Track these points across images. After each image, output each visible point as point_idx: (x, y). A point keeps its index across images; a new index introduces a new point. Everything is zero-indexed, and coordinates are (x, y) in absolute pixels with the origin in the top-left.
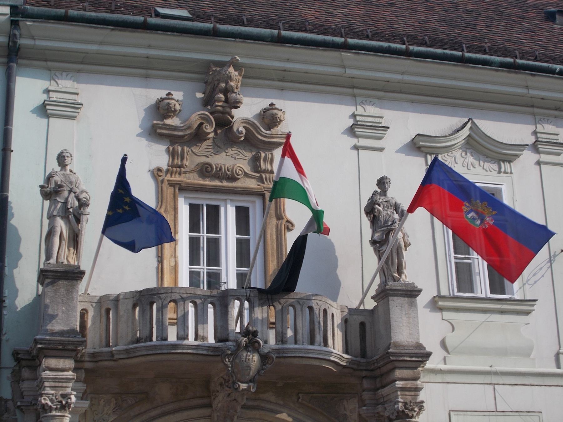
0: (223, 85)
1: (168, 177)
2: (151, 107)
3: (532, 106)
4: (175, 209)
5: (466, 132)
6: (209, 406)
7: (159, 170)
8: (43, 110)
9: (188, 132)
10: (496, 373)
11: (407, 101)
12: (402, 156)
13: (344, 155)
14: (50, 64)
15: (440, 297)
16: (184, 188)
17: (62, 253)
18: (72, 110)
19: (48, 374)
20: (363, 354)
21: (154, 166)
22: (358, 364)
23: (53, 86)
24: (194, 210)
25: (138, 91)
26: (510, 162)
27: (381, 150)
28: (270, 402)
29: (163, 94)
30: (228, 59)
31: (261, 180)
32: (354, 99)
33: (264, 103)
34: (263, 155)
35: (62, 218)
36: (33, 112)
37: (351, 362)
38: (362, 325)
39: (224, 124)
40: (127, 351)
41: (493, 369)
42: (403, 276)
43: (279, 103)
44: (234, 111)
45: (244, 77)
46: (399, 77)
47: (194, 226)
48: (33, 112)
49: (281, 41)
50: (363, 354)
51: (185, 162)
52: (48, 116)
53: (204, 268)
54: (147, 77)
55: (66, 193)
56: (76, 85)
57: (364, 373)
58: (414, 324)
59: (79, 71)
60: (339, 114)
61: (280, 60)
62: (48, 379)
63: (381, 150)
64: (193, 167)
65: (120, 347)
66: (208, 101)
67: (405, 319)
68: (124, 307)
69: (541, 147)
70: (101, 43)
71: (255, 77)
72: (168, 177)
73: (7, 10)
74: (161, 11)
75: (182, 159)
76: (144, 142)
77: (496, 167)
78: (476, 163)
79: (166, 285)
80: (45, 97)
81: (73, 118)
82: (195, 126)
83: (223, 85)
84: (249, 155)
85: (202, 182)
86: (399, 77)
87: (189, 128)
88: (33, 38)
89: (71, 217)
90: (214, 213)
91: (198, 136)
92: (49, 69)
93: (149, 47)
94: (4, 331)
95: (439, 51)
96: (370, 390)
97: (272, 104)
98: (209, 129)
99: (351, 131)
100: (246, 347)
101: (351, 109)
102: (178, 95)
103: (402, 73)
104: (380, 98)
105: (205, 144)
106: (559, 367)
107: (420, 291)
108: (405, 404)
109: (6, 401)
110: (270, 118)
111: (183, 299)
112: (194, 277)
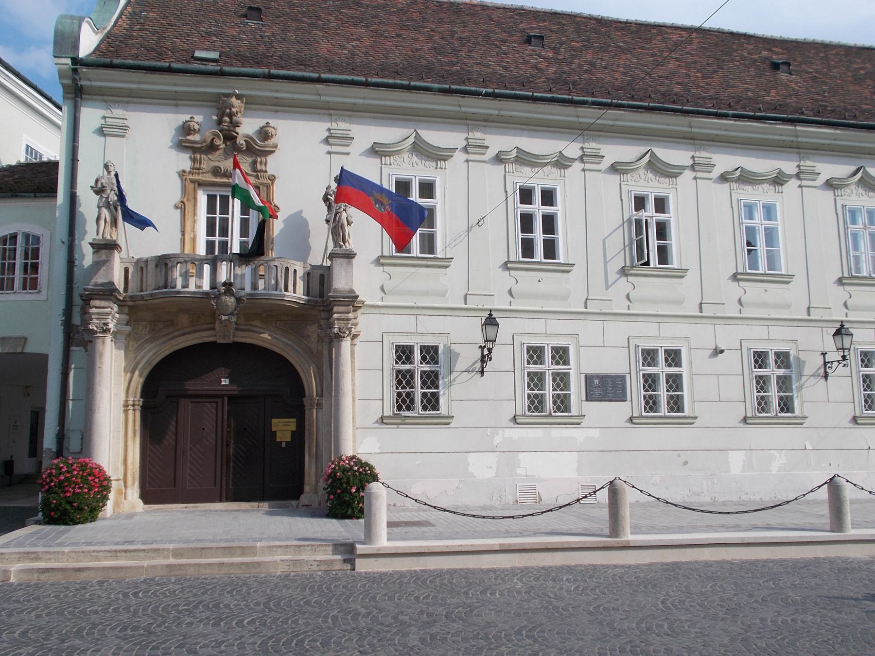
0: (228, 111)
1: (190, 177)
2: (179, 127)
3: (466, 119)
4: (195, 199)
5: (859, 175)
6: (214, 329)
7: (184, 171)
8: (101, 132)
9: (204, 144)
10: (418, 308)
11: (370, 117)
12: (364, 158)
13: (301, 159)
14: (106, 98)
15: (382, 257)
16: (201, 184)
17: (106, 232)
18: (122, 131)
19: (94, 310)
20: (321, 295)
21: (180, 169)
22: (317, 302)
23: (108, 113)
24: (211, 199)
25: (171, 116)
26: (445, 161)
27: (348, 154)
28: (256, 326)
29: (187, 117)
30: (230, 91)
31: (257, 177)
32: (330, 117)
33: (261, 122)
34: (259, 159)
35: (106, 208)
36: (94, 132)
37: (308, 301)
38: (322, 276)
39: (230, 137)
40: (151, 295)
41: (416, 305)
42: (347, 244)
43: (273, 122)
44: (237, 130)
45: (246, 103)
46: (361, 101)
47: (211, 209)
48: (94, 132)
49: (270, 77)
50: (321, 295)
51: (202, 165)
52: (105, 135)
53: (217, 239)
54: (177, 105)
55: (109, 191)
56: (125, 113)
57: (322, 308)
58: (350, 275)
59: (127, 102)
60: (318, 128)
61: (271, 91)
62: (94, 314)
63: (348, 154)
64: (209, 169)
65: (148, 292)
66: (220, 122)
67: (343, 273)
68: (151, 266)
69: (802, 176)
70: (139, 83)
71: (252, 104)
72: (190, 177)
73: (69, 61)
74: (198, 54)
75: (200, 163)
76: (174, 152)
77: (434, 164)
78: (419, 162)
79: (186, 252)
80: (103, 122)
81: (123, 136)
82: (209, 140)
83: (228, 111)
84: (250, 160)
85: (214, 180)
86: (361, 101)
87: (205, 141)
88: (89, 80)
89: (112, 207)
90: (225, 200)
91: (212, 148)
92: (105, 101)
93: (175, 85)
94: (75, 281)
95: (391, 81)
96: (325, 319)
97: (267, 123)
98: (219, 142)
99: (326, 141)
100: (225, 293)
101: (328, 125)
102: (199, 118)
103: (364, 99)
104: (350, 116)
105: (218, 153)
106: (586, 308)
107: (355, 254)
108: (340, 328)
109: (77, 326)
110: (264, 134)
111: (186, 262)
112: (210, 245)
